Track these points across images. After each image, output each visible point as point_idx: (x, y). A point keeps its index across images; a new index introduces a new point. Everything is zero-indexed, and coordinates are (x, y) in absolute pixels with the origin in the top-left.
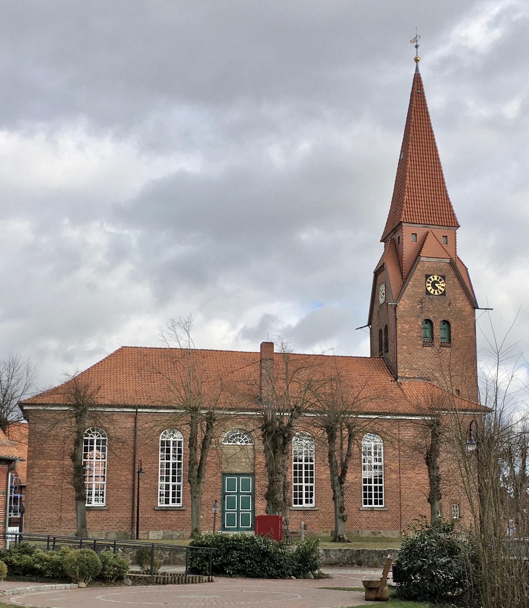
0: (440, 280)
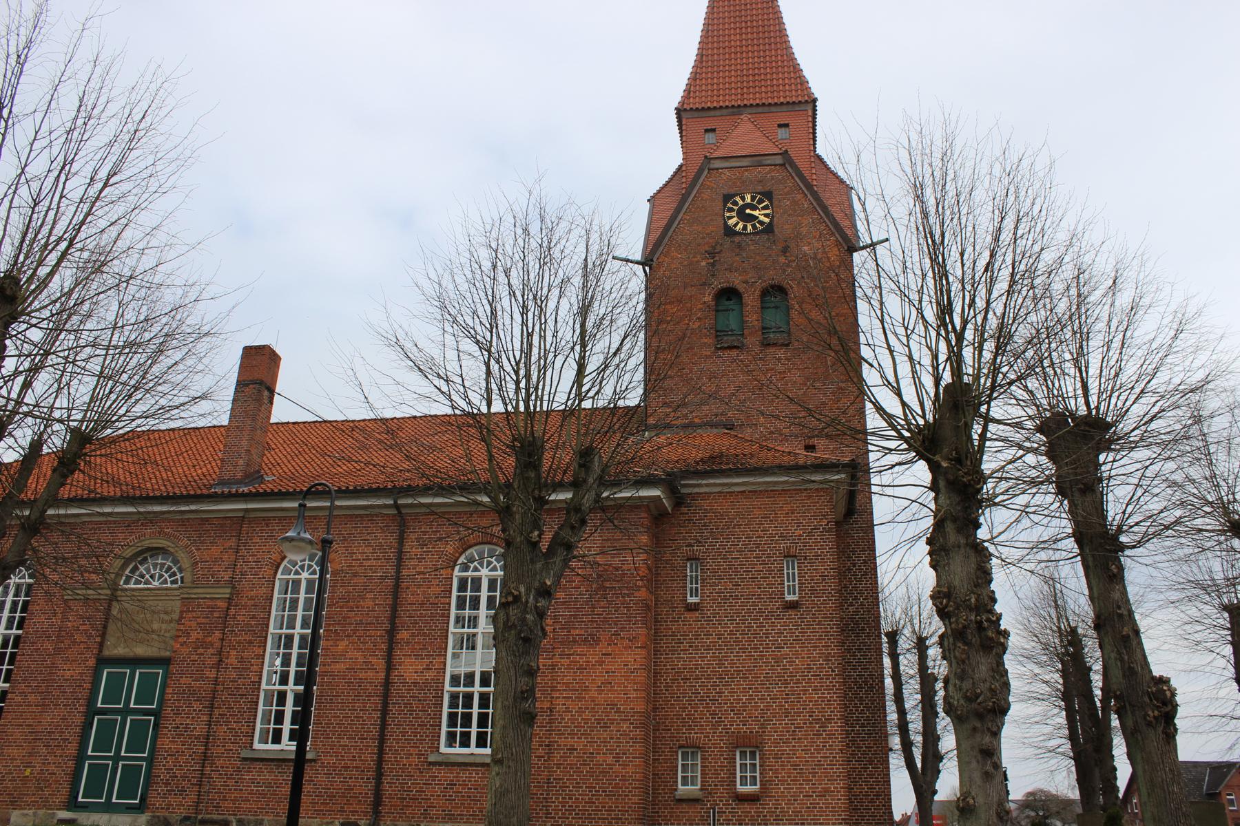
0: (761, 201)
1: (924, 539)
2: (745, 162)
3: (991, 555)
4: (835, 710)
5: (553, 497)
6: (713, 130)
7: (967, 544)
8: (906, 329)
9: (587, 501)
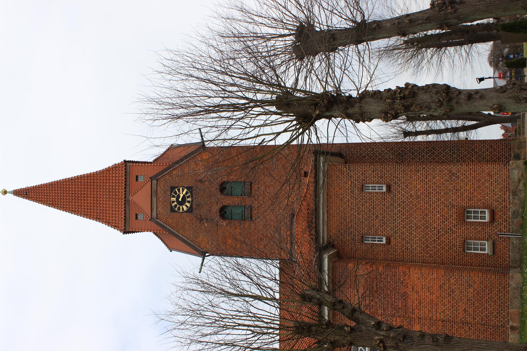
0: (176, 193)
1: (356, 124)
2: (154, 200)
3: (365, 90)
4: (445, 168)
5: (327, 318)
6: (136, 215)
7: (360, 103)
8: (246, 127)
9: (329, 299)
